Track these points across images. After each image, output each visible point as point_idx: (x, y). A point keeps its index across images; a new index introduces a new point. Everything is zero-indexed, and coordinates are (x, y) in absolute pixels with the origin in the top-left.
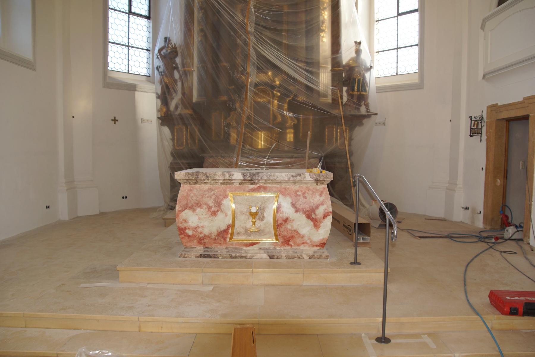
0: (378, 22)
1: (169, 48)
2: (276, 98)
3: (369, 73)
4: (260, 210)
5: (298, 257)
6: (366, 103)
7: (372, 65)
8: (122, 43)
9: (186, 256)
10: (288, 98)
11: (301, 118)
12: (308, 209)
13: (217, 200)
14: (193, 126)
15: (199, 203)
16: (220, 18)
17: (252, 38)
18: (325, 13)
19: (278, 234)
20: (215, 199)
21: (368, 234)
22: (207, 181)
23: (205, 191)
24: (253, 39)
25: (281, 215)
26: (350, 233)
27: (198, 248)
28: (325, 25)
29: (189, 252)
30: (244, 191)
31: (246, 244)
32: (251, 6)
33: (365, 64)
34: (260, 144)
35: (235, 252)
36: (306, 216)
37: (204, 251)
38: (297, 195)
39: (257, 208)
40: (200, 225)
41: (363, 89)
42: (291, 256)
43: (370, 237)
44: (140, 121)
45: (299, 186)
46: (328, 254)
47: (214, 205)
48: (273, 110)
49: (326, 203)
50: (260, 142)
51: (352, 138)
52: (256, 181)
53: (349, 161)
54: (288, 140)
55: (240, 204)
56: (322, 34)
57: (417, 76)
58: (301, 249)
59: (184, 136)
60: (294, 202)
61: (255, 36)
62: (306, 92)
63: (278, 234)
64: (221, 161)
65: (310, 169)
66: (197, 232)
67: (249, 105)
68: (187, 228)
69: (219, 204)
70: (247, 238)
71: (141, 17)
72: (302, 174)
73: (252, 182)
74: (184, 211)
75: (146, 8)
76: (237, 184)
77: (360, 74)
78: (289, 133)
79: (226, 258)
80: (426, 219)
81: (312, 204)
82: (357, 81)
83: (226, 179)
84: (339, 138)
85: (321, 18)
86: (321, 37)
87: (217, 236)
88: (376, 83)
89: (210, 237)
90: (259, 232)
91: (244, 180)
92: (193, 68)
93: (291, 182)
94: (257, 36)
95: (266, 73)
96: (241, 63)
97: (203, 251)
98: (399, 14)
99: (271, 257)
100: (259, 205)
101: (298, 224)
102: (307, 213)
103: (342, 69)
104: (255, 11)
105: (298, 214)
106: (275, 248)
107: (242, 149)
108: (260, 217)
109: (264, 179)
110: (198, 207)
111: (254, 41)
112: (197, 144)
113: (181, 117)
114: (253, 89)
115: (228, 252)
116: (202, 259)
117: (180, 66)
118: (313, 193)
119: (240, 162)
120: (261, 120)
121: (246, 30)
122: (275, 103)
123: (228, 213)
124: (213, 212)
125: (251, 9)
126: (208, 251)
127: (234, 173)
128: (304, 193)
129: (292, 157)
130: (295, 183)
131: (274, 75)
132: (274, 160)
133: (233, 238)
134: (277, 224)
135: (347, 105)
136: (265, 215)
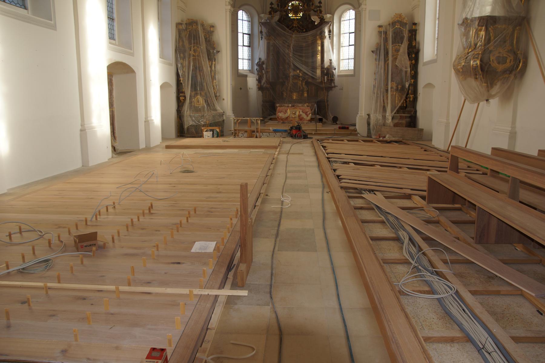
17: (292, 59)
44: (249, 88)
57: (353, 71)
69: (286, 111)
78: (305, 93)
85: (318, 50)
98: (350, 45)
131: (299, 72)
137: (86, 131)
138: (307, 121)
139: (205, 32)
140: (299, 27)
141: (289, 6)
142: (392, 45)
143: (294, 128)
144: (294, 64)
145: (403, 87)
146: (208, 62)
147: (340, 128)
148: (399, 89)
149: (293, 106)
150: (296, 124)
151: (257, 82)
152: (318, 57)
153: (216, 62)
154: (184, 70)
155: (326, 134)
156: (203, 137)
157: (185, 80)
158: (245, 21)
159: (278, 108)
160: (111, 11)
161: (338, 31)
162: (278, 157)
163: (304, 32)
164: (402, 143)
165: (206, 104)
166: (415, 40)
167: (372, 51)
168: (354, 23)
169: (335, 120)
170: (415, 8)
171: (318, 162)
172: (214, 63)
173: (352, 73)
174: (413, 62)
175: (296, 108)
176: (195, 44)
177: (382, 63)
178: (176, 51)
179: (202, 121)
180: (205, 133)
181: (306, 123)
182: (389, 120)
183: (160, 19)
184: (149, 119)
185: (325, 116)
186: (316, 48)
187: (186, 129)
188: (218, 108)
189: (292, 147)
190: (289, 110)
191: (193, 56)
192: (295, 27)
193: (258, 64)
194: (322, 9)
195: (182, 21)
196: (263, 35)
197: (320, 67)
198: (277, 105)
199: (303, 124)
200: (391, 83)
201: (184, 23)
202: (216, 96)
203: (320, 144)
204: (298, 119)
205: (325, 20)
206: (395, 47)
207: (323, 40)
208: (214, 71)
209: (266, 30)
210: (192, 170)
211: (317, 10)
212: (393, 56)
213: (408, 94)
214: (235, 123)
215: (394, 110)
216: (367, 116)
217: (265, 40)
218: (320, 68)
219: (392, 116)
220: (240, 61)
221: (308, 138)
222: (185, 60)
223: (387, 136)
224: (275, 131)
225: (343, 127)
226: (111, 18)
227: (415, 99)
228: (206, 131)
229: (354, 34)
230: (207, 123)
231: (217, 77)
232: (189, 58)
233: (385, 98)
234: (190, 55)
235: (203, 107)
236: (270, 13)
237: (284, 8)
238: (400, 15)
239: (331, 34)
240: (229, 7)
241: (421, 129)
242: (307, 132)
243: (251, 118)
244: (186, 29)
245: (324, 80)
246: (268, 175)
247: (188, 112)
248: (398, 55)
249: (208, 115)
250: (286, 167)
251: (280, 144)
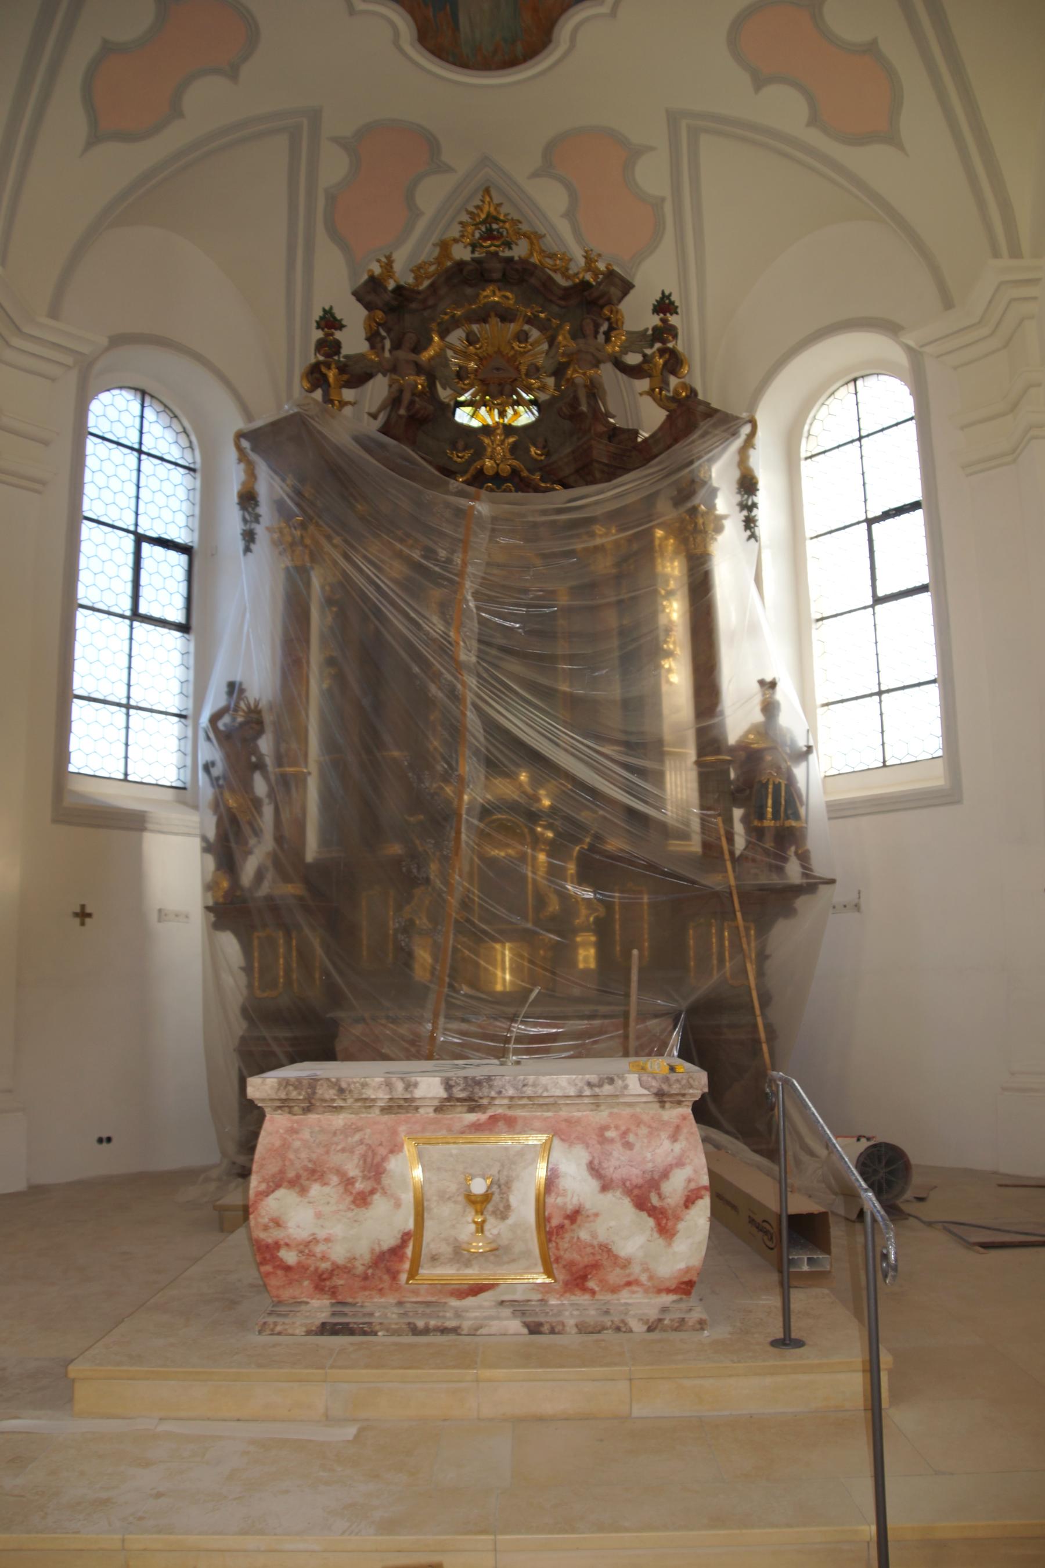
0: (820, 623)
1: (241, 713)
2: (543, 847)
3: (804, 765)
4: (496, 1186)
5: (614, 1326)
6: (800, 852)
7: (811, 743)
8: (109, 698)
9: (279, 1328)
10: (577, 846)
11: (616, 900)
12: (640, 1181)
13: (369, 1160)
14: (307, 931)
15: (318, 1169)
16: (382, 629)
17: (472, 681)
18: (671, 605)
19: (552, 1260)
20: (364, 1157)
21: (824, 1246)
22: (342, 1103)
23: (335, 1134)
24: (475, 682)
25: (560, 1200)
26: (770, 1244)
27: (315, 1303)
28: (673, 639)
29: (285, 1316)
30: (450, 1130)
31: (458, 1290)
32: (465, 592)
33: (793, 742)
34: (499, 980)
35: (424, 1315)
36: (633, 1200)
37: (334, 1314)
38: (603, 1140)
39: (489, 1181)
40: (322, 1234)
41: (789, 812)
42: (592, 1323)
43: (828, 1251)
44: (154, 916)
45: (611, 1114)
46: (704, 1316)
47: (361, 1174)
48: (534, 881)
49: (692, 1160)
50: (499, 973)
51: (768, 952)
52: (485, 1102)
53: (760, 1020)
54: (581, 966)
55: (439, 1169)
56: (666, 664)
57: (939, 768)
58: (623, 1301)
59: (281, 961)
60: (596, 1162)
61: (479, 676)
62: (628, 827)
63: (552, 1260)
64: (388, 1032)
65: (642, 1060)
66: (311, 1254)
67: (466, 868)
68: (282, 1242)
69: (375, 1171)
70: (461, 1272)
71: (164, 627)
72: (618, 1076)
73: (473, 1104)
74: (273, 1191)
75: (180, 602)
76: (427, 1112)
77: (779, 769)
78: (585, 944)
79: (399, 1335)
80: (1000, 1186)
81: (650, 1166)
82: (770, 790)
83: (396, 1097)
84: (727, 954)
85: (662, 620)
86: (663, 672)
87: (370, 1267)
88: (825, 792)
89: (349, 1272)
90: (497, 1252)
91: (449, 1099)
92: (306, 766)
93: (586, 1100)
94: (485, 675)
95: (511, 776)
96: (441, 750)
97: (329, 1313)
98: (878, 600)
99: (534, 1329)
100: (494, 1171)
101: (611, 1227)
102: (636, 1192)
103: (728, 758)
104: (478, 608)
105: (609, 1196)
107: (448, 996)
108: (498, 1209)
109: (507, 1095)
110: (315, 1180)
111: (477, 689)
112: (318, 982)
113: (272, 905)
114: (476, 822)
115: (405, 1314)
116: (328, 1337)
117: (269, 761)
118: (653, 1132)
119: (444, 1034)
120: (501, 912)
121: (454, 659)
122: (540, 860)
123: (403, 1196)
124: (359, 1193)
125: (467, 601)
126: (345, 1315)
127: (419, 1079)
128: (625, 1134)
129: (592, 1016)
130: (598, 1105)
131: (536, 782)
132: (542, 1025)
133: (417, 1273)
134: (548, 1229)
135: (747, 858)
136: (513, 1200)
140: (525, 474)
151: (210, 861)
207: (705, 547)
209: (284, 480)
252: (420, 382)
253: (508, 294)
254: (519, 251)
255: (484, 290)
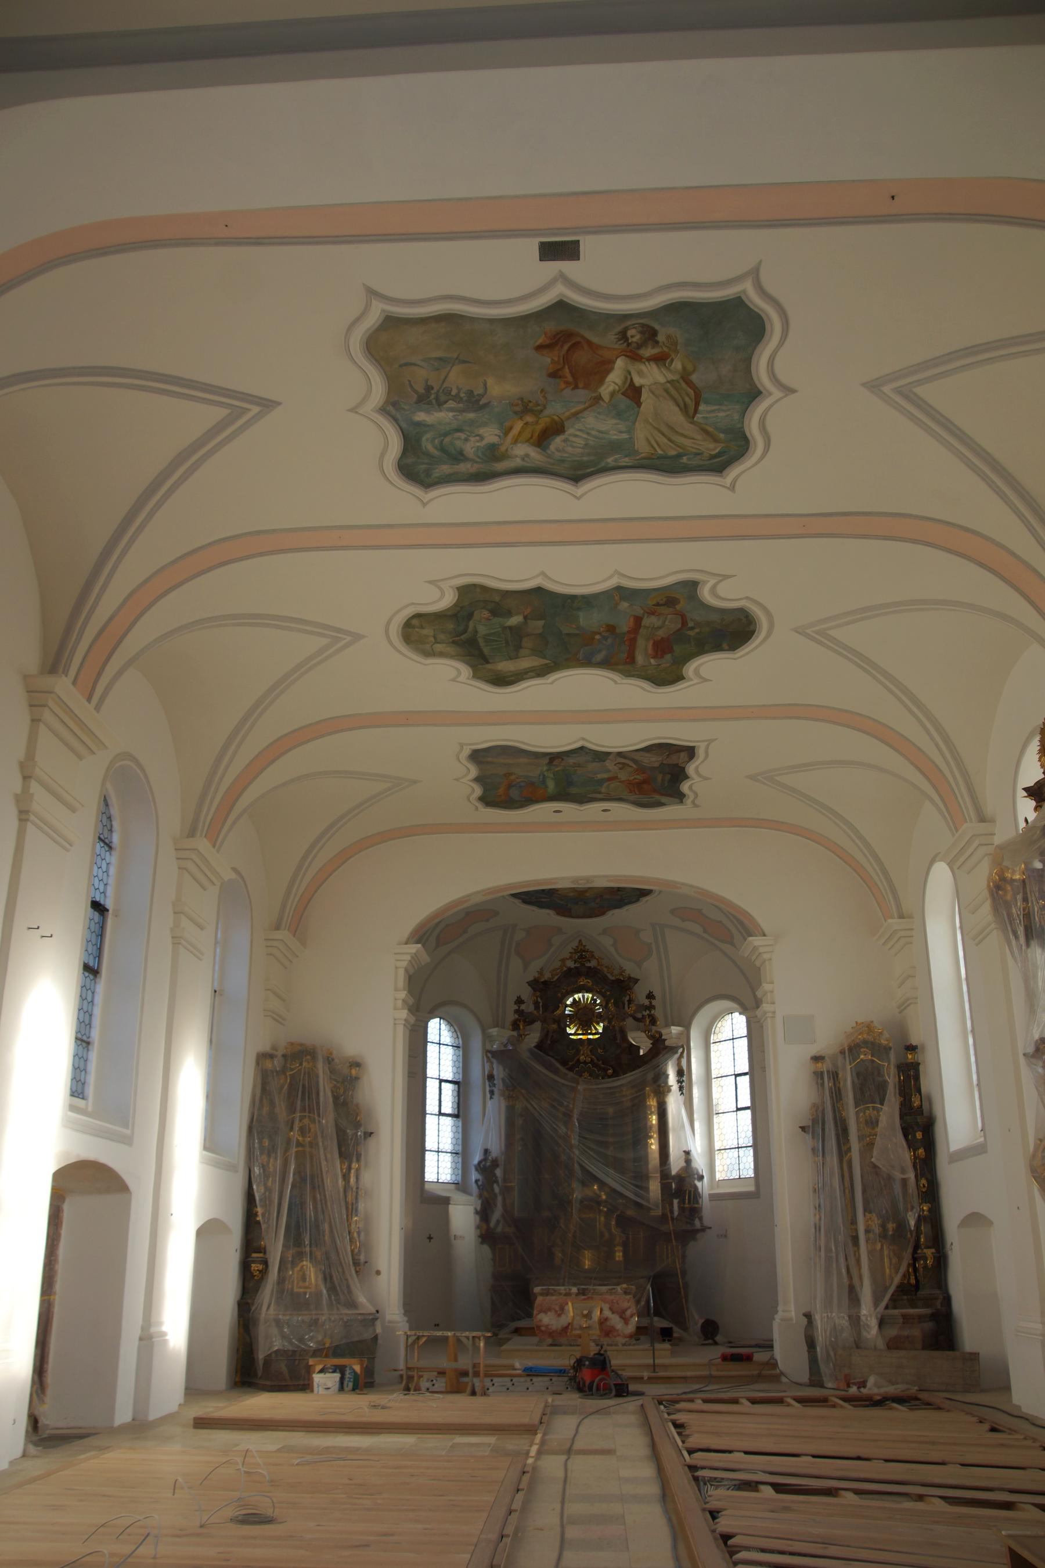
17: (577, 1152)
18: (652, 1117)
44: (453, 1238)
57: (753, 1182)
73: (584, 1294)
85: (649, 1124)
86: (649, 1145)
98: (738, 1109)
106: (599, 1340)
117: (500, 1180)
125: (575, 1122)
131: (600, 1189)
136: (593, 1316)
137: (153, 1340)
138: (626, 1337)
139: (336, 1080)
141: (567, 1006)
142: (856, 1108)
143: (587, 1363)
144: (581, 1166)
145: (901, 1226)
146: (338, 1162)
147: (725, 1358)
148: (890, 1233)
149: (582, 1292)
150: (593, 1350)
151: (478, 1218)
152: (652, 1144)
153: (363, 1163)
154: (270, 1183)
155: (685, 1379)
156: (312, 1391)
157: (269, 1214)
158: (447, 1045)
159: (539, 1299)
160: (82, 1068)
161: (702, 1071)
162: (539, 1463)
163: (609, 1077)
164: (917, 1402)
165: (326, 1288)
166: (919, 1091)
167: (800, 1127)
168: (746, 1048)
169: (710, 1330)
170: (908, 1006)
171: (663, 1484)
172: (355, 1165)
173: (752, 1188)
174: (921, 1151)
175: (592, 1298)
176: (305, 1112)
177: (833, 1159)
178: (250, 1129)
179: (311, 1339)
180: (317, 1378)
181: (624, 1345)
182: (872, 1331)
183: (214, 1041)
184: (153, 1330)
185: (679, 1318)
186: (646, 1119)
187: (261, 1363)
188: (362, 1299)
189: (581, 1429)
190: (570, 1304)
191: (299, 1144)
192: (585, 1063)
193: (481, 1168)
194: (658, 1013)
195: (274, 1048)
196: (494, 1085)
197: (657, 1173)
198: (537, 1290)
199: (614, 1348)
200: (865, 1216)
201: (279, 1053)
202: (356, 1263)
203: (666, 1416)
204: (598, 1332)
205: (667, 1043)
206: (864, 1113)
208: (354, 1189)
209: (504, 1070)
210: (269, 1512)
211: (643, 1015)
212: (861, 1138)
213: (917, 1247)
214: (409, 1347)
215: (884, 1296)
216: (805, 1320)
217: (502, 1098)
218: (658, 1175)
219: (879, 1316)
220: (430, 1159)
221: (629, 1394)
222: (273, 1155)
223: (871, 1381)
224: (531, 1372)
225: (732, 1355)
226: (83, 1041)
227: (941, 1261)
228: (321, 1371)
229: (747, 1077)
230: (327, 1345)
231: (361, 1206)
232: (286, 1150)
233: (852, 1262)
234: (288, 1141)
235: (318, 1295)
236: (515, 1026)
237: (553, 1011)
238: (869, 1027)
239: (683, 1081)
240: (404, 1014)
241: (971, 1354)
242: (626, 1374)
243: (458, 1334)
244: (284, 1071)
245: (672, 1211)
246: (504, 1533)
247: (271, 1311)
248: (876, 1135)
249: (330, 1319)
250: (563, 1502)
251: (545, 1418)
252: (555, 1026)
253: (589, 981)
254: (593, 964)
255: (579, 979)
